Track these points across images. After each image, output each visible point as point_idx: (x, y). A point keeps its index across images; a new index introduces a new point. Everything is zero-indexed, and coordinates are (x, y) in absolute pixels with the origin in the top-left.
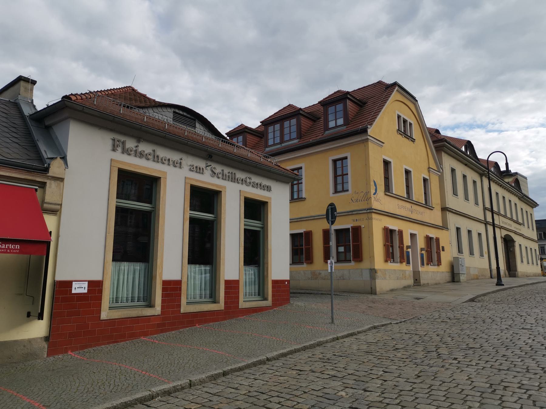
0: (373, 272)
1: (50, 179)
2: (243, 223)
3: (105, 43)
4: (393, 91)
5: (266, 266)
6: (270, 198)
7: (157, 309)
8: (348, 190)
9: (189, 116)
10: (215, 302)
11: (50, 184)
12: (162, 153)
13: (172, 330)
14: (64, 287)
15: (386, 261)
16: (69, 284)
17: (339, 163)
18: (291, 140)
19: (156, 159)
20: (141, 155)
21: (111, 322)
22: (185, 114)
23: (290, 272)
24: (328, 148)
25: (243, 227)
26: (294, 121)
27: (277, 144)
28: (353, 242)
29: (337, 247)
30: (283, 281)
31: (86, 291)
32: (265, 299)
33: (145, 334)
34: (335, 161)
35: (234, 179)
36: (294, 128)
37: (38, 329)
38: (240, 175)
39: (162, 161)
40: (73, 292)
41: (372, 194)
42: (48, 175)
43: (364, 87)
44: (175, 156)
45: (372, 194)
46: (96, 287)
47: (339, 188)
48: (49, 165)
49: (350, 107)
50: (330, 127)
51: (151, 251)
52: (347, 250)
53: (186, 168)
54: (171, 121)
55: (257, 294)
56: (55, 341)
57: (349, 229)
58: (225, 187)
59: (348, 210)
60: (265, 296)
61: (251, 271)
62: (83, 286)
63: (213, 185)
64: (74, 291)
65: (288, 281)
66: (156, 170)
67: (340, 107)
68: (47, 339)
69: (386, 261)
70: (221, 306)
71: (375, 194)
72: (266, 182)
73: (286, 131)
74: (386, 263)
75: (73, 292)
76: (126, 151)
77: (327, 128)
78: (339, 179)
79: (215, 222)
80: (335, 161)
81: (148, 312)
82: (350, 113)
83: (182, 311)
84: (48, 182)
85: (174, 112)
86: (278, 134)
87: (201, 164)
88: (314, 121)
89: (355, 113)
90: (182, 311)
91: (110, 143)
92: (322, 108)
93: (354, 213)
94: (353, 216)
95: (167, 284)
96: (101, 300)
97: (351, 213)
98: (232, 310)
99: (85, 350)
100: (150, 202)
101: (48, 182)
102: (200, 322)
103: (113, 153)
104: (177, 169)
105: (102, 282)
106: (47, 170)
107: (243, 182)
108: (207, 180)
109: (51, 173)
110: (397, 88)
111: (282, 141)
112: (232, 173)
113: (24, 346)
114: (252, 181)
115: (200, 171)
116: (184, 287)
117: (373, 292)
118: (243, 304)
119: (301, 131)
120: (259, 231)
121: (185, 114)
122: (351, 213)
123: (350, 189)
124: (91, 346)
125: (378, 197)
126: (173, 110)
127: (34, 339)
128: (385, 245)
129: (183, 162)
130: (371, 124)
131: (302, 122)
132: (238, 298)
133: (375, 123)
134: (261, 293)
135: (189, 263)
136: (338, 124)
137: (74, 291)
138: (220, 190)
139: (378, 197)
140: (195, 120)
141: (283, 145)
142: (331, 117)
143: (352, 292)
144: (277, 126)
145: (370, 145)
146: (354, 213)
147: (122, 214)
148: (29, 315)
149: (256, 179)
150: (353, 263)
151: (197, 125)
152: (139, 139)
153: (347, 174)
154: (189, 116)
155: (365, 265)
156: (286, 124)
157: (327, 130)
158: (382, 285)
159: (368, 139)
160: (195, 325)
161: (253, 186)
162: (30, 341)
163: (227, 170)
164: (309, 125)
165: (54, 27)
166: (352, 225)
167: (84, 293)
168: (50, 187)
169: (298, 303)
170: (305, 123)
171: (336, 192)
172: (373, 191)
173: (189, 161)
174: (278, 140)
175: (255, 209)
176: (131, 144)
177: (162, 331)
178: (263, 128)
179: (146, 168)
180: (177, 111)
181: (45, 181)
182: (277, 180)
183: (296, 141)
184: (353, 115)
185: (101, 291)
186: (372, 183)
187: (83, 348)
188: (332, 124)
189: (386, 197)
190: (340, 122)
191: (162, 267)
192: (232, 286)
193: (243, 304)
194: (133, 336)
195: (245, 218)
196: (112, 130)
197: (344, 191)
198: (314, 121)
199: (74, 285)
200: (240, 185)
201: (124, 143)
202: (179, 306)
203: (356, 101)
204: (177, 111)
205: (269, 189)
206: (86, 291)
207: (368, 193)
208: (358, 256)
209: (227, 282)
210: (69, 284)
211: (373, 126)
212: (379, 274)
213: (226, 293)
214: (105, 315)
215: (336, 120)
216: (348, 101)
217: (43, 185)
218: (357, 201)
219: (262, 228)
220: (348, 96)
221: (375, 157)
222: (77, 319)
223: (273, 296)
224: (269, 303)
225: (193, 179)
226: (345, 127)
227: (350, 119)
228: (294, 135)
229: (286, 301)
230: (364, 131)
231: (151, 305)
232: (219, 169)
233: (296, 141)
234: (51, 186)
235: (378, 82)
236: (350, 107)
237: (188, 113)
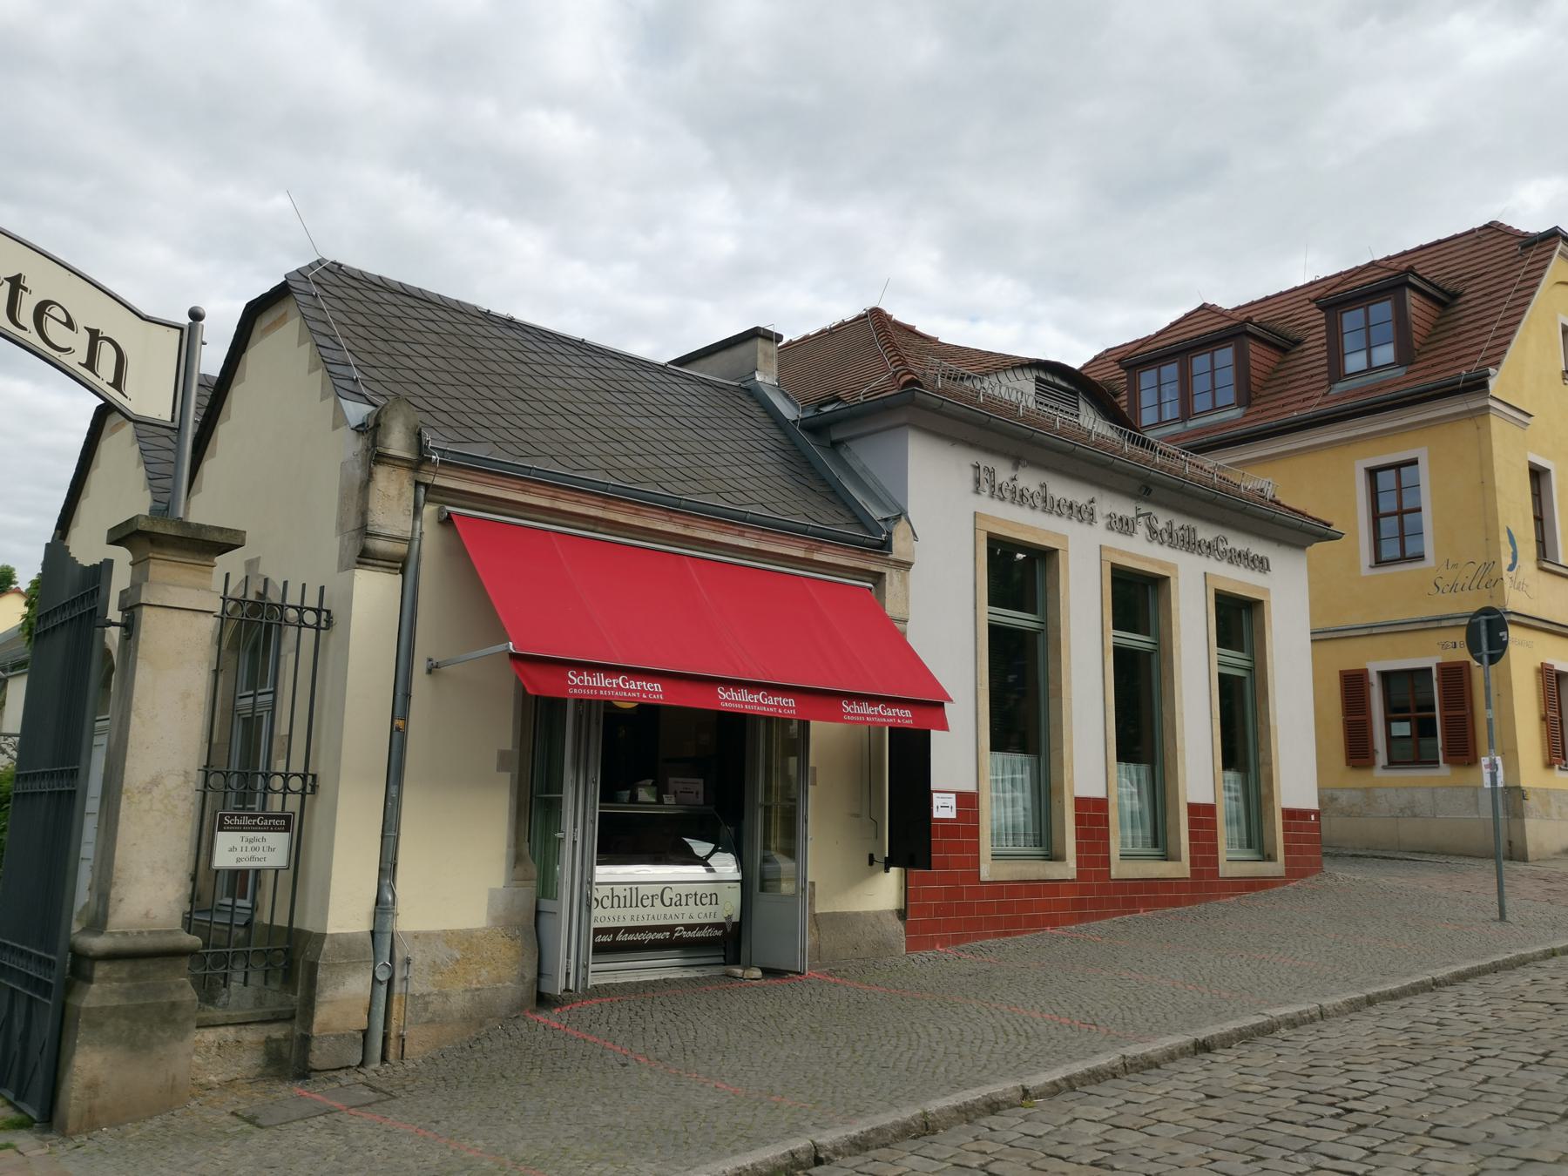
0: (1513, 798)
1: (891, 567)
2: (1215, 659)
4: (1550, 257)
5: (1263, 771)
6: (1267, 591)
8: (1420, 557)
9: (1064, 384)
10: (1165, 858)
12: (1062, 490)
13: (1099, 917)
15: (1549, 765)
17: (1386, 480)
18: (1215, 409)
19: (1050, 506)
20: (1020, 498)
21: (997, 887)
22: (1058, 381)
23: (1319, 789)
24: (1352, 433)
25: (1216, 670)
26: (1225, 356)
27: (1173, 421)
28: (1444, 707)
29: (1388, 722)
30: (1304, 814)
32: (1270, 858)
33: (1055, 924)
34: (1372, 473)
35: (1190, 544)
36: (1227, 376)
38: (1205, 533)
41: (1505, 567)
43: (1439, 242)
44: (1079, 494)
45: (1505, 567)
47: (1390, 549)
48: (889, 534)
49: (1414, 310)
50: (1348, 371)
51: (1167, 737)
52: (1425, 728)
53: (1101, 523)
54: (1032, 404)
57: (1430, 669)
58: (1175, 567)
59: (1424, 615)
60: (1267, 850)
61: (1017, 764)
65: (1317, 814)
67: (1382, 310)
68: (902, 914)
69: (1549, 765)
70: (1181, 869)
71: (1511, 568)
72: (1258, 548)
73: (1200, 383)
74: (1549, 772)
76: (997, 492)
77: (1336, 372)
78: (1389, 525)
79: (1040, 639)
80: (1372, 473)
82: (1415, 327)
84: (887, 571)
85: (1038, 379)
86: (1171, 392)
87: (1126, 508)
88: (1284, 351)
89: (1429, 327)
90: (1114, 874)
91: (969, 474)
92: (1319, 317)
93: (1444, 623)
94: (1442, 632)
97: (1435, 624)
98: (1205, 883)
99: (962, 946)
101: (887, 571)
102: (1149, 904)
103: (975, 497)
104: (1084, 527)
106: (886, 546)
107: (1210, 549)
108: (1142, 552)
110: (1561, 245)
111: (1186, 413)
117: (1517, 853)
118: (1226, 869)
119: (1248, 383)
121: (1058, 381)
122: (1435, 624)
123: (1429, 549)
125: (1520, 579)
126: (1035, 373)
128: (1544, 719)
129: (1097, 508)
130: (1497, 364)
131: (1252, 356)
133: (1507, 359)
134: (1256, 841)
135: (992, 749)
136: (1376, 363)
139: (1520, 579)
141: (1191, 424)
142: (1349, 342)
143: (1448, 854)
144: (1171, 370)
145: (1496, 423)
146: (1444, 623)
147: (998, 635)
148: (871, 860)
149: (1237, 542)
150: (1444, 771)
151: (1082, 404)
152: (1017, 461)
153: (1419, 510)
154: (1064, 384)
155: (1487, 772)
156: (1200, 362)
157: (1339, 380)
158: (1541, 833)
159: (1488, 407)
161: (1231, 561)
163: (1179, 522)
164: (1271, 364)
165: (348, 74)
166: (1440, 660)
169: (1343, 874)
170: (1259, 355)
171: (1379, 562)
172: (1506, 560)
174: (1170, 411)
175: (1237, 619)
176: (1003, 473)
177: (1082, 918)
178: (1113, 372)
179: (1033, 530)
180: (1043, 375)
182: (1280, 541)
183: (1235, 413)
184: (1424, 332)
186: (1504, 537)
187: (957, 941)
188: (1355, 362)
189: (1542, 575)
190: (1385, 354)
192: (1093, 813)
193: (1226, 869)
195: (1115, 628)
196: (971, 445)
197: (1403, 559)
198: (1284, 351)
200: (1203, 559)
201: (992, 472)
203: (1438, 295)
204: (1043, 375)
205: (1261, 565)
207: (1491, 564)
208: (1463, 751)
209: (1081, 803)
211: (1502, 368)
212: (1532, 802)
214: (987, 871)
215: (1369, 349)
216: (1409, 293)
217: (878, 578)
218: (1453, 589)
219: (1249, 670)
220: (1411, 279)
221: (1509, 456)
223: (1287, 850)
224: (1277, 868)
226: (1401, 372)
227: (1416, 345)
228: (1228, 395)
229: (1317, 868)
230: (1478, 384)
231: (1053, 855)
232: (1162, 519)
233: (1235, 413)
234: (892, 577)
235: (1486, 227)
236: (1414, 310)
237: (1063, 379)
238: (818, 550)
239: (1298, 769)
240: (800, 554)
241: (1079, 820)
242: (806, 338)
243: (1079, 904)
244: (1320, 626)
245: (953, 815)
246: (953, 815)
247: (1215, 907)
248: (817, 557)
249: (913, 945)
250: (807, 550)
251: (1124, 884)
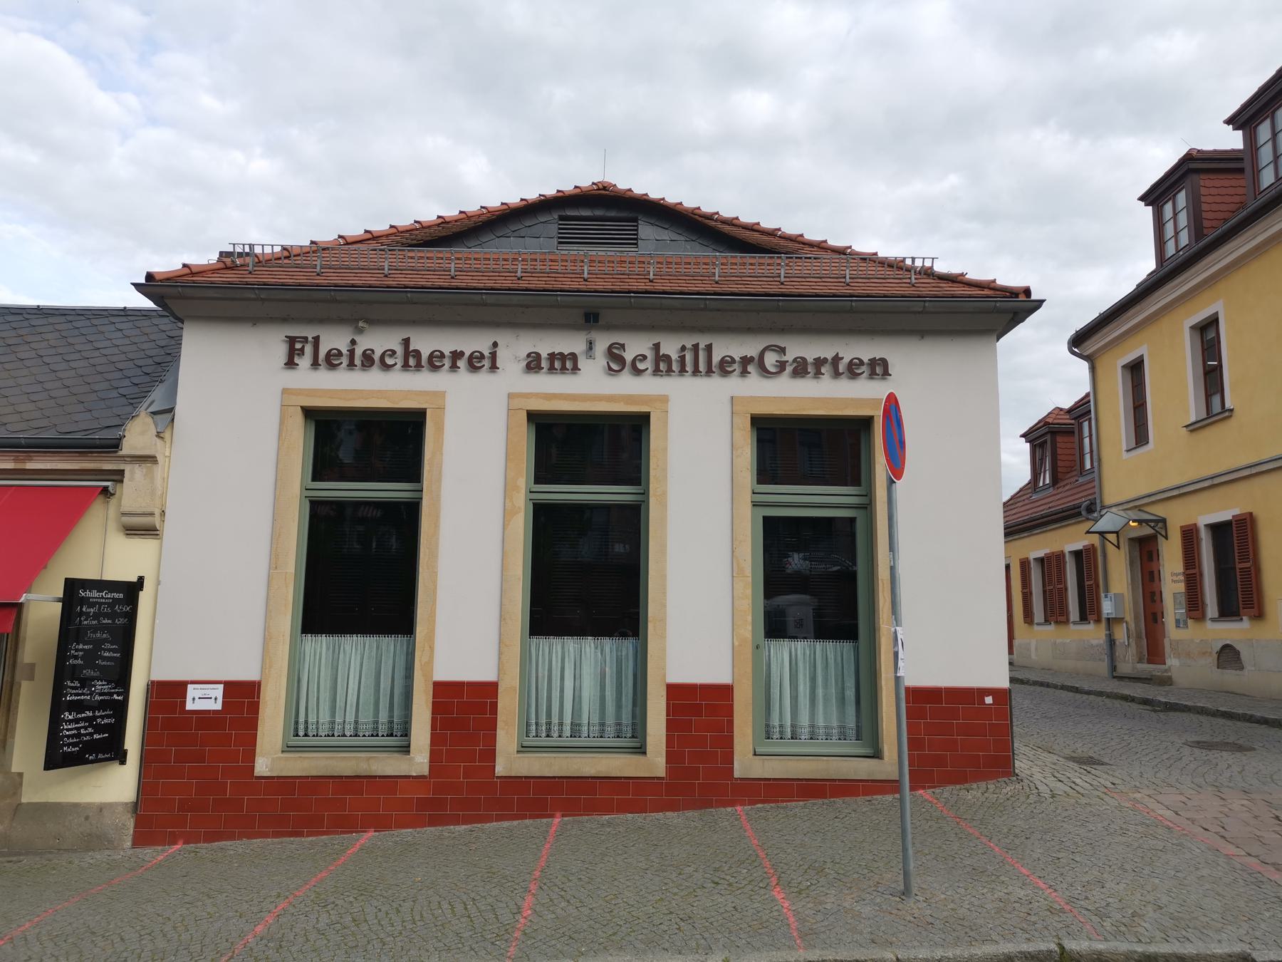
1: (131, 462)
2: (747, 498)
3: (1102, 53)
7: (419, 760)
11: (132, 473)
14: (167, 695)
16: (179, 689)
19: (412, 360)
22: (599, 213)
30: (970, 696)
31: (218, 706)
37: (117, 785)
38: (726, 347)
39: (434, 362)
40: (188, 708)
42: (121, 453)
46: (242, 696)
55: (852, 733)
56: (155, 818)
62: (213, 694)
63: (610, 398)
64: (190, 706)
66: (408, 394)
72: (865, 350)
75: (188, 708)
81: (389, 765)
83: (501, 769)
84: (128, 468)
90: (501, 769)
95: (446, 693)
96: (256, 729)
100: (856, 482)
101: (128, 468)
103: (290, 374)
104: (483, 378)
105: (259, 683)
108: (592, 387)
109: (127, 448)
112: (696, 347)
113: (87, 818)
114: (789, 357)
115: (564, 363)
116: (508, 706)
120: (852, 521)
124: (231, 837)
127: (111, 806)
132: (728, 743)
137: (190, 706)
138: (644, 409)
140: (636, 220)
154: (613, 214)
160: (552, 816)
162: (101, 808)
167: (215, 712)
168: (132, 479)
173: (514, 348)
176: (335, 339)
181: (121, 467)
185: (255, 708)
191: (432, 648)
194: (346, 824)
196: (285, 320)
199: (192, 691)
202: (490, 755)
205: (879, 369)
206: (218, 706)
210: (179, 689)
213: (671, 726)
222: (206, 772)
225: (537, 395)
238: (23, 461)
239: (948, 610)
240: (10, 465)
241: (437, 708)
242: (990, 286)
243: (423, 804)
244: (1015, 519)
245: (218, 706)
246: (218, 706)
247: (724, 815)
248: (30, 466)
249: (144, 837)
250: (16, 460)
251: (517, 783)
